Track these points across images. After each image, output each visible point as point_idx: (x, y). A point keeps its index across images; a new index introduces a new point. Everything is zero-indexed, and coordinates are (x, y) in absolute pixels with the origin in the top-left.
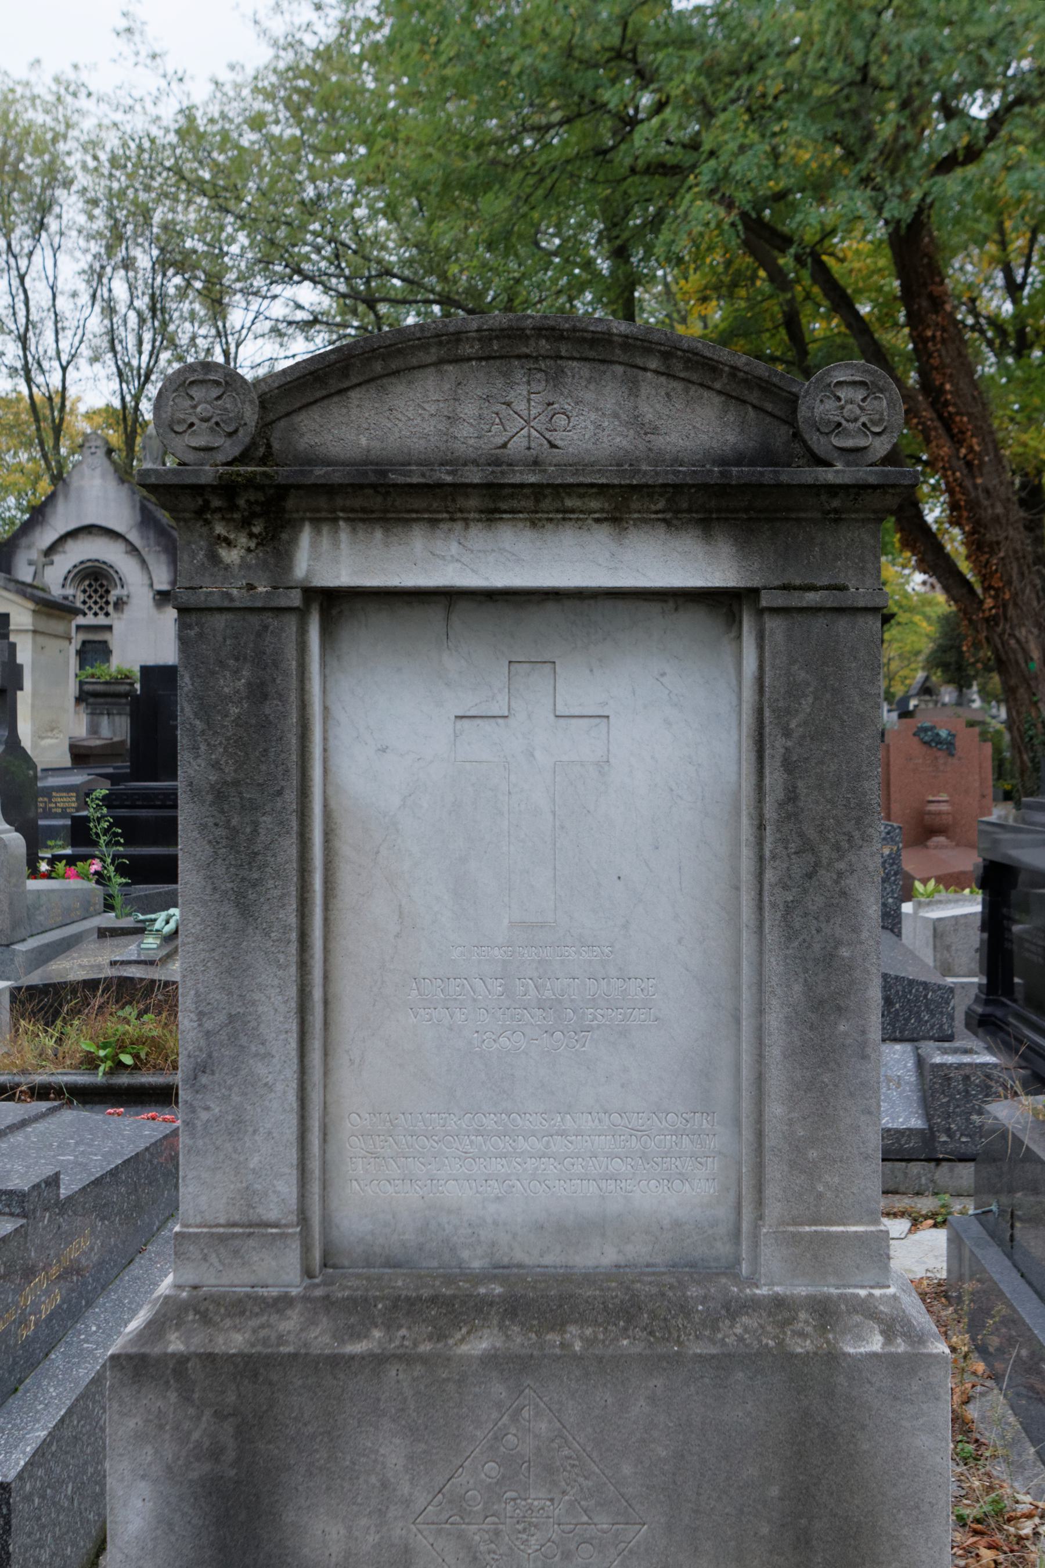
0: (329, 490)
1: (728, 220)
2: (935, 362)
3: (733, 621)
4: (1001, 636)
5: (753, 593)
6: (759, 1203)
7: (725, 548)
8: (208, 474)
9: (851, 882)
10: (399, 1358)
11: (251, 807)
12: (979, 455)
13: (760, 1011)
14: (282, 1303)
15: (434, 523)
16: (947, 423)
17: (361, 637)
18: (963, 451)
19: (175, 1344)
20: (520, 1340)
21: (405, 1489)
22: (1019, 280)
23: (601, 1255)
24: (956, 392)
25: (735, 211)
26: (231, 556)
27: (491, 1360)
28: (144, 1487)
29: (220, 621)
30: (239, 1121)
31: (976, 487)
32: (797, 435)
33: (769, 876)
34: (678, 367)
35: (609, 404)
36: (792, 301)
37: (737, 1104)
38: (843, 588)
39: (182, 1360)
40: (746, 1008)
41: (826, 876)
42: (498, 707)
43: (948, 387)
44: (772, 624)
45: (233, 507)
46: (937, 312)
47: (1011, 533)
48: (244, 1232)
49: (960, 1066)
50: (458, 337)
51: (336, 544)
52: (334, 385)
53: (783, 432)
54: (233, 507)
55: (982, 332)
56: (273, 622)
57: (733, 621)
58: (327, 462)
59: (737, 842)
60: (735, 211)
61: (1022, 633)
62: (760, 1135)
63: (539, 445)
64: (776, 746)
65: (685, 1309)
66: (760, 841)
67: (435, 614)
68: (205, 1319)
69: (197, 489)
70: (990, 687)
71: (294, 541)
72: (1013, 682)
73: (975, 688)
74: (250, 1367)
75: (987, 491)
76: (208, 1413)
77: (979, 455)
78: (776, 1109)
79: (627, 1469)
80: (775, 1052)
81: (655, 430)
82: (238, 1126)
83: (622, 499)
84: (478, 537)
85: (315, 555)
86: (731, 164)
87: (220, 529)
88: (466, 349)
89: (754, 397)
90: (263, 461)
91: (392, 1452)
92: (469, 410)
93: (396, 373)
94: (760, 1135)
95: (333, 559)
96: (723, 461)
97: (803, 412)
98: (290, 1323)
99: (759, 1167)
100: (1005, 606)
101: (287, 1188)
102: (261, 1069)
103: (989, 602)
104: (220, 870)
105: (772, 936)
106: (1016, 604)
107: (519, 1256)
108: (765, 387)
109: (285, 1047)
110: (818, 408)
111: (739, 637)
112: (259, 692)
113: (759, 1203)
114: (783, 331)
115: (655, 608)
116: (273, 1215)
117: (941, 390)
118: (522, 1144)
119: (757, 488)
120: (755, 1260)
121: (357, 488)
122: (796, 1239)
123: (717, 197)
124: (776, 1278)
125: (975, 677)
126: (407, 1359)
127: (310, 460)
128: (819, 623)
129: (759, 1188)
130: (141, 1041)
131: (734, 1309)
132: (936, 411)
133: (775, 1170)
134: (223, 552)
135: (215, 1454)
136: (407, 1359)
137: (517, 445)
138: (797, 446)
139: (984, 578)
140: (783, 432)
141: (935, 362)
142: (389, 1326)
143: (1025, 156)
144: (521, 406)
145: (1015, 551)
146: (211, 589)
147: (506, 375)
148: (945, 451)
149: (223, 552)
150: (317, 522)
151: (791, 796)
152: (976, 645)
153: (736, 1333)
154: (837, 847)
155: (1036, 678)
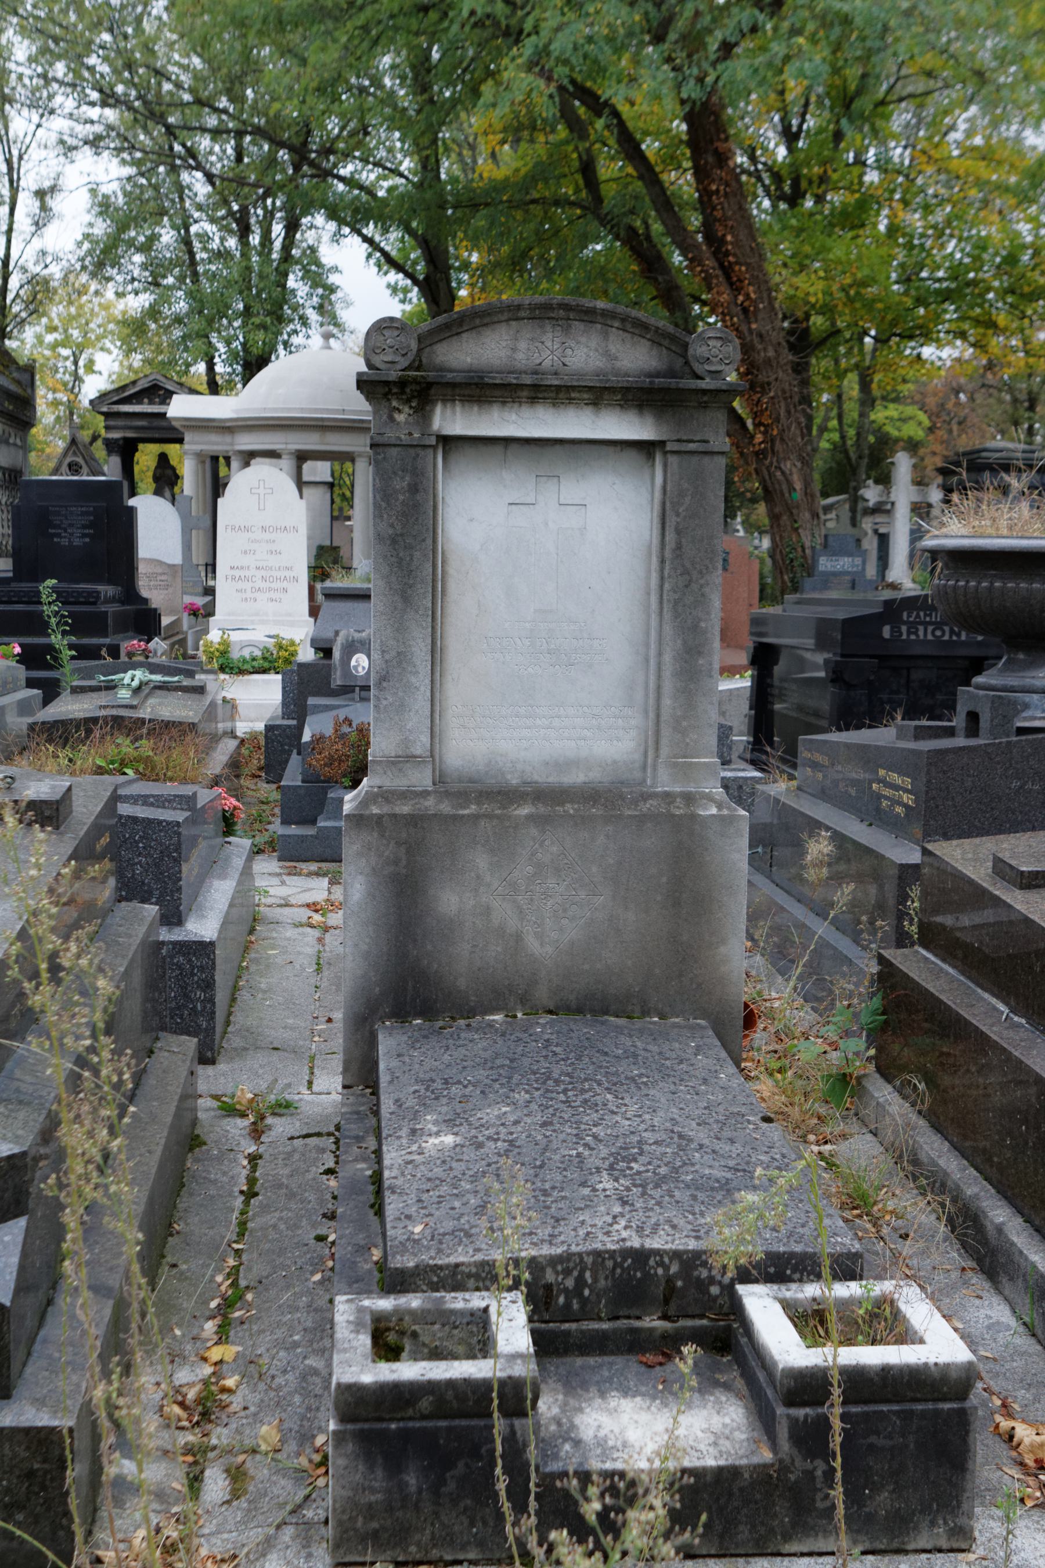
0: (453, 385)
1: (547, 92)
2: (718, 214)
3: (650, 457)
4: (768, 468)
5: (662, 443)
6: (657, 749)
7: (650, 420)
8: (393, 375)
9: (707, 590)
10: (485, 816)
11: (409, 547)
12: (755, 302)
13: (660, 654)
14: (425, 794)
15: (504, 403)
16: (727, 271)
17: (462, 459)
18: (741, 298)
19: (375, 810)
20: (542, 809)
21: (488, 879)
22: (794, 129)
23: (576, 778)
24: (736, 243)
25: (553, 84)
26: (400, 418)
27: (529, 817)
28: (361, 878)
29: (394, 451)
30: (402, 705)
31: (750, 330)
32: (687, 363)
33: (667, 586)
34: (629, 326)
35: (593, 344)
36: (588, 151)
37: (646, 702)
38: (707, 442)
39: (380, 817)
40: (653, 652)
41: (694, 586)
42: (530, 499)
43: (729, 238)
44: (673, 459)
45: (403, 392)
46: (721, 168)
47: (781, 374)
48: (404, 760)
49: (736, 779)
50: (519, 307)
51: (454, 413)
52: (455, 330)
53: (680, 362)
54: (403, 392)
55: (759, 179)
56: (421, 453)
57: (650, 457)
58: (451, 371)
59: (649, 571)
60: (553, 84)
61: (787, 466)
62: (658, 716)
63: (557, 363)
64: (672, 521)
65: (622, 797)
66: (662, 570)
67: (499, 449)
68: (387, 800)
69: (387, 383)
70: (753, 517)
71: (432, 411)
72: (777, 510)
73: (739, 519)
74: (414, 821)
75: (760, 336)
76: (392, 844)
77: (755, 302)
78: (667, 702)
79: (594, 869)
80: (667, 674)
81: (616, 359)
82: (402, 708)
83: (599, 394)
84: (526, 411)
85: (443, 418)
86: (550, 43)
87: (395, 403)
88: (522, 314)
89: (666, 343)
90: (418, 369)
91: (481, 861)
92: (523, 345)
93: (486, 325)
94: (658, 716)
95: (452, 420)
96: (650, 375)
97: (691, 352)
98: (430, 802)
99: (657, 732)
100: (773, 441)
101: (425, 739)
102: (413, 680)
103: (759, 438)
104: (393, 579)
105: (667, 615)
106: (782, 440)
107: (536, 778)
108: (672, 338)
109: (424, 669)
110: (698, 350)
111: (653, 465)
112: (414, 489)
113: (657, 749)
114: (579, 177)
115: (611, 449)
116: (418, 752)
117: (722, 241)
118: (538, 722)
119: (666, 390)
120: (654, 777)
121: (468, 385)
122: (675, 765)
123: (537, 69)
124: (665, 782)
125: (739, 508)
126: (490, 817)
127: (442, 369)
128: (695, 459)
129: (657, 743)
130: (138, 760)
131: (645, 797)
132: (717, 260)
133: (666, 732)
134: (396, 416)
135: (396, 862)
136: (490, 817)
137: (547, 363)
138: (687, 369)
139: (755, 415)
140: (680, 362)
141: (718, 214)
142: (479, 804)
143: (805, 48)
144: (549, 344)
145: (784, 391)
146: (391, 435)
147: (542, 327)
148: (725, 298)
149: (396, 416)
150: (444, 401)
151: (679, 547)
152: (747, 477)
153: (645, 807)
154: (701, 572)
155: (798, 507)
